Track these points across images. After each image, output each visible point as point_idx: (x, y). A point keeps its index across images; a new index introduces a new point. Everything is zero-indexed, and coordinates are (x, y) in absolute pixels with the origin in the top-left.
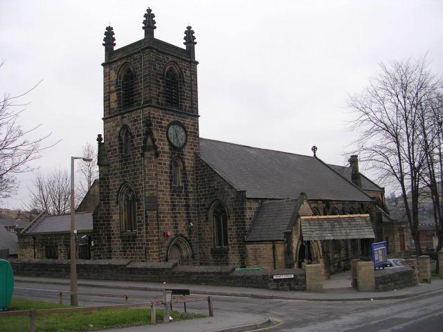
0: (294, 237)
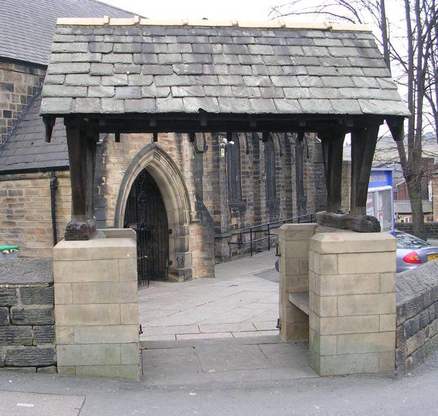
0: (113, 159)
